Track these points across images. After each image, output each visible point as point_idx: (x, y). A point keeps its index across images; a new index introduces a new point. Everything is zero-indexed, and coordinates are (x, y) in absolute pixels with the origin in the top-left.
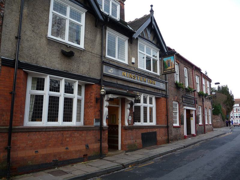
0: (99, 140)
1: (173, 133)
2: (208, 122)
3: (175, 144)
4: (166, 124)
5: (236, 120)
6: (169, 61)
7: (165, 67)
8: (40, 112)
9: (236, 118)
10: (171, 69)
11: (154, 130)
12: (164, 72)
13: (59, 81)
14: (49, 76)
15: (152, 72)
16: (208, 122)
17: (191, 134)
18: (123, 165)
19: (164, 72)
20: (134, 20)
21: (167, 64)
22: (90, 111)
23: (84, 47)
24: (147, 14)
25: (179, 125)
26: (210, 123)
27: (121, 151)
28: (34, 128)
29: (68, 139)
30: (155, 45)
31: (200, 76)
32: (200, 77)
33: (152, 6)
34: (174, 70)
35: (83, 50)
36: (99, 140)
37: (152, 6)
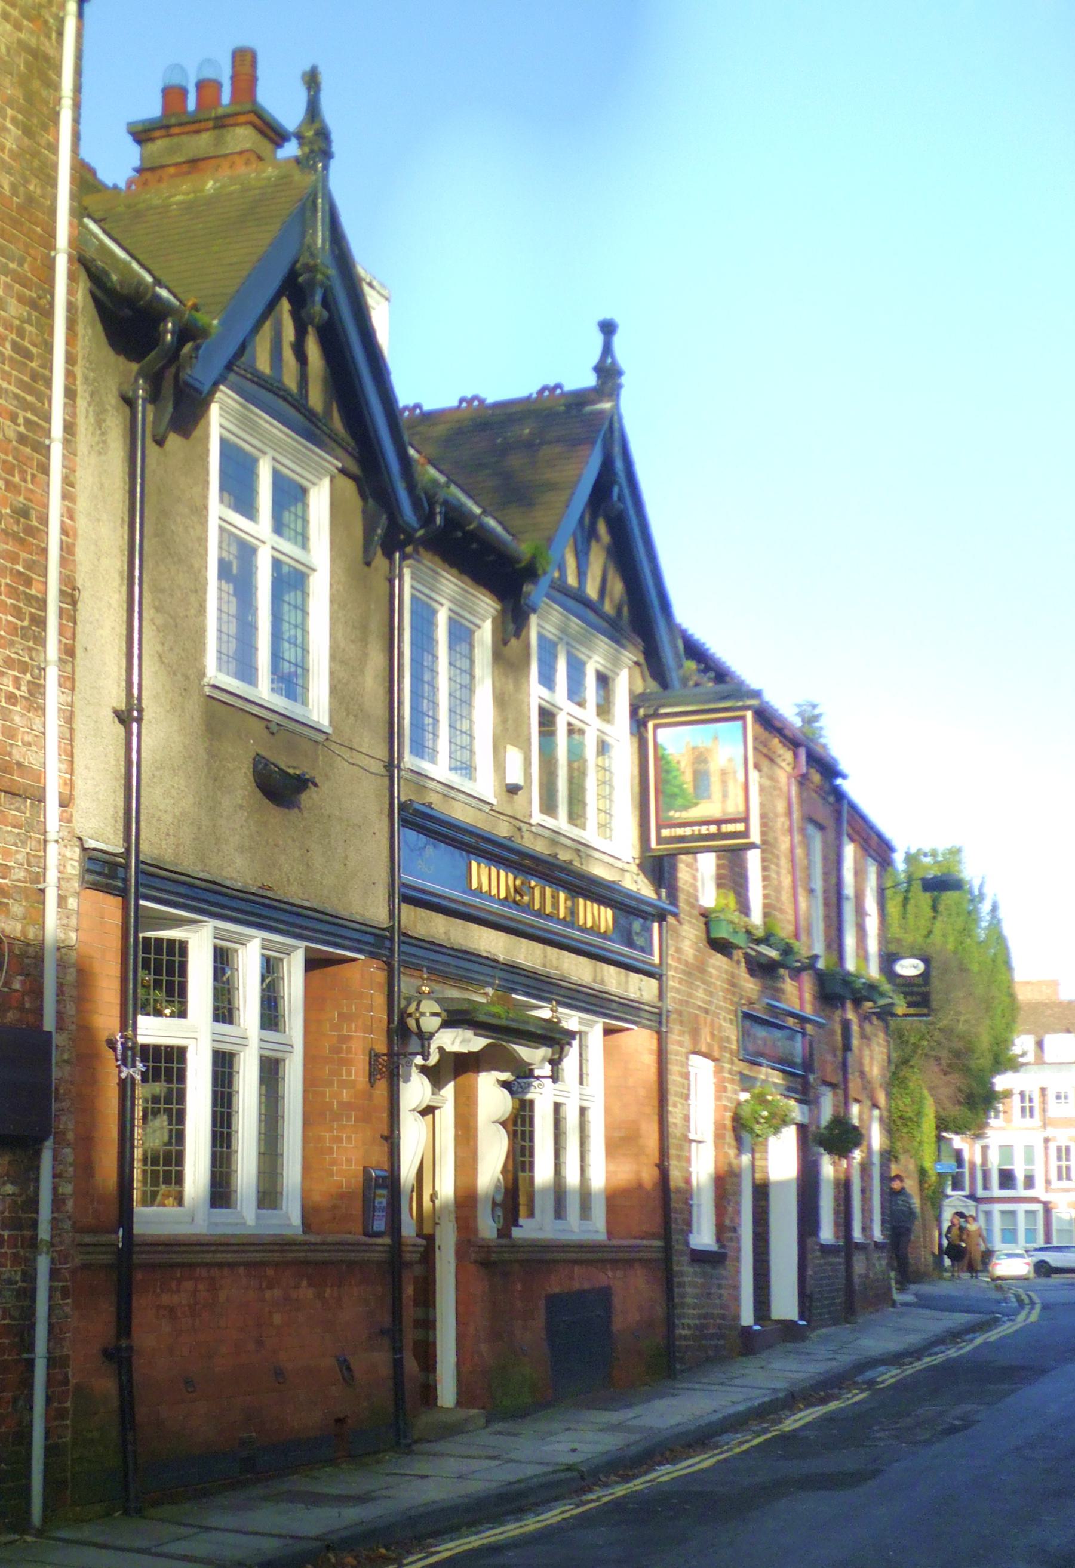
0: (383, 1332)
1: (689, 1300)
2: (866, 1229)
3: (722, 1384)
4: (653, 1236)
5: (997, 1207)
6: (700, 758)
7: (674, 796)
8: (527, 1159)
9: (996, 1192)
10: (718, 822)
11: (603, 1278)
12: (665, 833)
13: (276, 958)
14: (216, 928)
15: (561, 822)
16: (866, 1229)
17: (770, 1319)
18: (703, 1444)
19: (665, 833)
20: (454, 403)
21: (688, 777)
22: (339, 1140)
23: (331, 722)
24: (570, 385)
25: (714, 1247)
26: (878, 1235)
27: (462, 1413)
28: (179, 1245)
29: (277, 1319)
30: (354, 457)
31: (829, 822)
32: (831, 835)
33: (608, 328)
34: (740, 827)
35: (321, 738)
36: (383, 1332)
37: (608, 328)
